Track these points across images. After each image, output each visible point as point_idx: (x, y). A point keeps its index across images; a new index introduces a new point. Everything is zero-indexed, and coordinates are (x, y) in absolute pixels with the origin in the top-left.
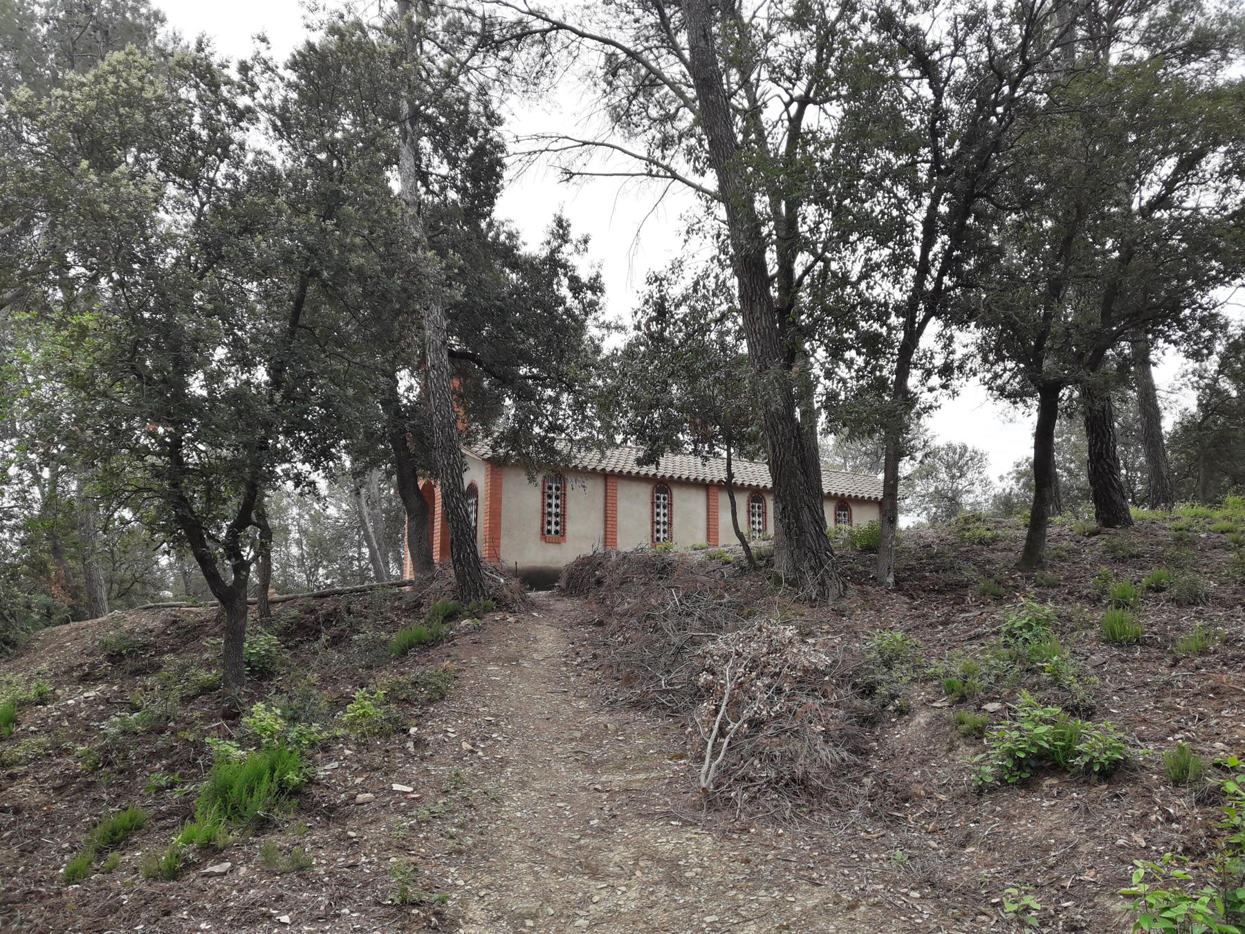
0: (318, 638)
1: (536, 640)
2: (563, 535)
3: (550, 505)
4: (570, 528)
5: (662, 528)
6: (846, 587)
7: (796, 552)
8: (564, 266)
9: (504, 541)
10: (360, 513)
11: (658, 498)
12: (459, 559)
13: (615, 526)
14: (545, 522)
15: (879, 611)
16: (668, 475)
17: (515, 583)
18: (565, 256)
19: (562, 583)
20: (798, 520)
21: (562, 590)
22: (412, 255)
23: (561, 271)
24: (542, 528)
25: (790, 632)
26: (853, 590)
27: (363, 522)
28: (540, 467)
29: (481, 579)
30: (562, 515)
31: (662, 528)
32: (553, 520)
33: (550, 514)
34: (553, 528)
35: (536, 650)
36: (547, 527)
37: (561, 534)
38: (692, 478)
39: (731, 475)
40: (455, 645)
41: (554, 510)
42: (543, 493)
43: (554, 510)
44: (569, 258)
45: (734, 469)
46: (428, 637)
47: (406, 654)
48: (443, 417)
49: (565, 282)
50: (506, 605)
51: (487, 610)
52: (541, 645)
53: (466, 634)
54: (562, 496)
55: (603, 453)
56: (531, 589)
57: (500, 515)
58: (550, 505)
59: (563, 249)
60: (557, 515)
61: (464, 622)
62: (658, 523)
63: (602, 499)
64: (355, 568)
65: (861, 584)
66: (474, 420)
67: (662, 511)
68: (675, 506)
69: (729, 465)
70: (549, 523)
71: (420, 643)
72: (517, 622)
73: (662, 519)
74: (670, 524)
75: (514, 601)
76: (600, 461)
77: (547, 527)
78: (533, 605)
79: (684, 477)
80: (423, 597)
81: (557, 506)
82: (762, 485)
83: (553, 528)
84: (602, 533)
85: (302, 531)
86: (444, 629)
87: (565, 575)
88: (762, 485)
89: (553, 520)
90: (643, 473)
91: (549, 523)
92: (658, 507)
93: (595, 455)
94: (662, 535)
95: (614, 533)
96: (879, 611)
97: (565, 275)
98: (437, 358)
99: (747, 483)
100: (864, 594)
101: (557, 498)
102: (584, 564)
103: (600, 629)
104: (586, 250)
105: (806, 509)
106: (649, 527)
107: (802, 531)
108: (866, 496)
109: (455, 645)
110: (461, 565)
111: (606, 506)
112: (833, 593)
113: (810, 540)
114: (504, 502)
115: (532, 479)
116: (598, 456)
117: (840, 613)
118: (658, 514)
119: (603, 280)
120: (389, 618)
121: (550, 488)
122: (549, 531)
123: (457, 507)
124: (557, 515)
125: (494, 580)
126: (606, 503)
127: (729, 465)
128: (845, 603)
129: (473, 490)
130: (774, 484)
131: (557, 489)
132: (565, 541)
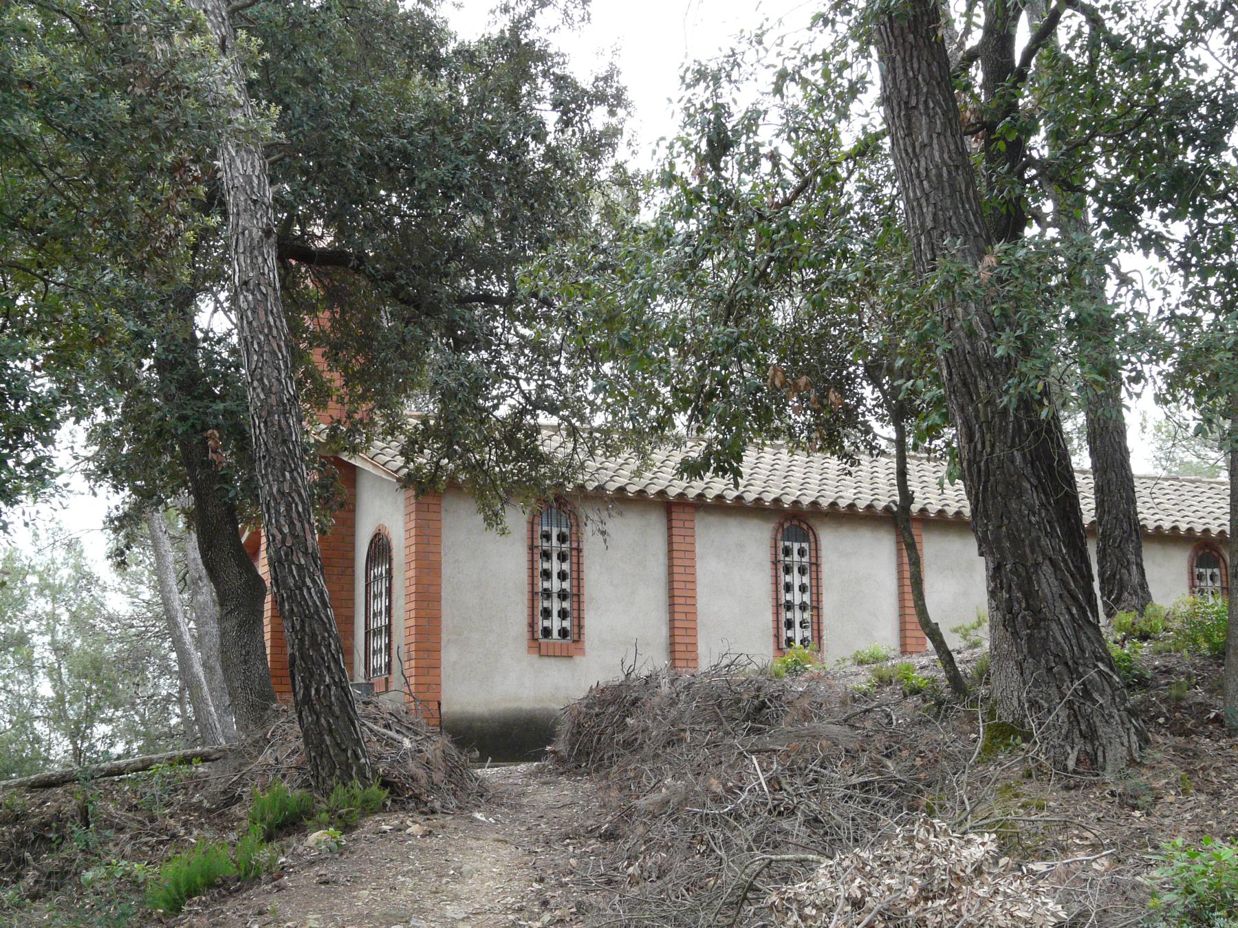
0: (19, 877)
1: (459, 876)
2: (578, 640)
3: (547, 574)
4: (593, 622)
5: (797, 616)
6: (1145, 741)
7: (1030, 663)
8: (542, 56)
9: (449, 656)
10: (166, 602)
11: (787, 552)
12: (307, 699)
13: (692, 615)
14: (537, 609)
15: (1216, 795)
16: (806, 501)
17: (438, 746)
18: (542, 34)
19: (561, 746)
20: (1029, 594)
21: (561, 760)
22: (160, 46)
23: (536, 69)
24: (532, 625)
25: (981, 847)
26: (1164, 743)
27: (172, 624)
28: (515, 490)
29: (358, 742)
30: (574, 596)
31: (797, 616)
32: (556, 606)
33: (547, 594)
34: (556, 624)
35: (456, 898)
36: (542, 623)
37: (573, 638)
38: (861, 505)
39: (907, 497)
40: (280, 888)
41: (555, 585)
42: (532, 548)
43: (555, 585)
44: (551, 38)
45: (914, 485)
46: (231, 871)
47: (179, 910)
48: (268, 392)
49: (546, 89)
50: (416, 797)
51: (370, 808)
52: (472, 884)
53: (312, 863)
54: (573, 555)
55: (643, 455)
56: (482, 761)
57: (438, 599)
58: (547, 574)
59: (537, 20)
60: (563, 596)
61: (315, 837)
62: (789, 606)
63: (662, 558)
64: (174, 721)
65: (1187, 734)
66: (363, 398)
67: (796, 579)
68: (825, 568)
69: (902, 473)
70: (789, 624)
71: (211, 885)
72: (429, 834)
73: (797, 597)
74: (817, 608)
75: (434, 787)
76: (638, 473)
77: (542, 623)
78: (485, 796)
79: (843, 503)
80: (241, 782)
81: (803, 589)
82: (1215, 530)
83: (556, 624)
84: (664, 631)
85: (60, 649)
86: (264, 854)
87: (564, 730)
88: (1215, 530)
89: (556, 606)
90: (692, 493)
91: (547, 613)
92: (788, 570)
93: (628, 459)
94: (798, 634)
95: (692, 631)
96: (1216, 795)
97: (545, 74)
98: (253, 265)
99: (1183, 527)
100: (1188, 756)
101: (802, 571)
102: (604, 703)
103: (610, 846)
104: (586, 18)
105: (1047, 568)
106: (769, 617)
107: (1038, 618)
108: (1167, 525)
109: (280, 888)
110: (312, 710)
111: (671, 573)
112: (1116, 754)
113: (1059, 634)
114: (446, 571)
115: (493, 519)
116: (635, 463)
117: (1129, 802)
118: (788, 588)
119: (622, 80)
120: (165, 830)
121: (547, 537)
122: (547, 632)
123: (301, 586)
124: (563, 596)
125: (390, 743)
126: (670, 567)
127: (902, 473)
128: (1142, 778)
129: (380, 549)
130: (974, 511)
131: (562, 538)
132: (582, 652)
